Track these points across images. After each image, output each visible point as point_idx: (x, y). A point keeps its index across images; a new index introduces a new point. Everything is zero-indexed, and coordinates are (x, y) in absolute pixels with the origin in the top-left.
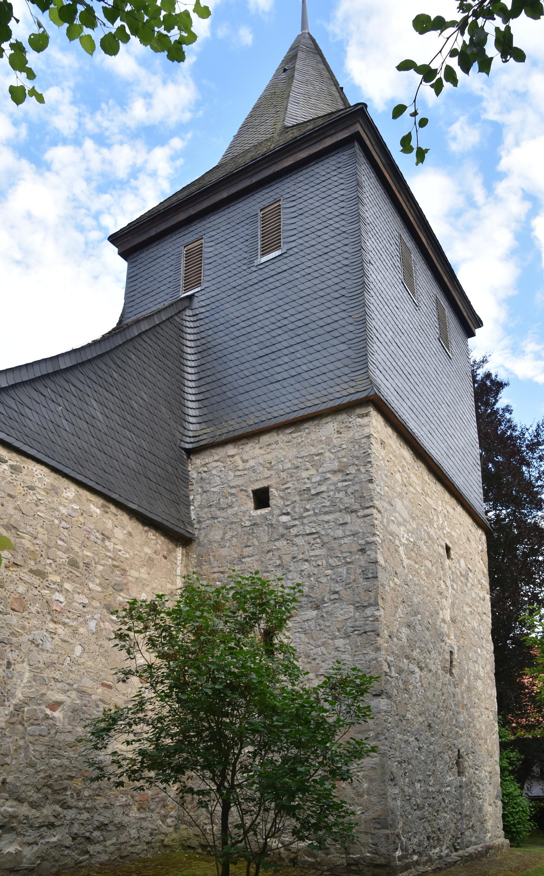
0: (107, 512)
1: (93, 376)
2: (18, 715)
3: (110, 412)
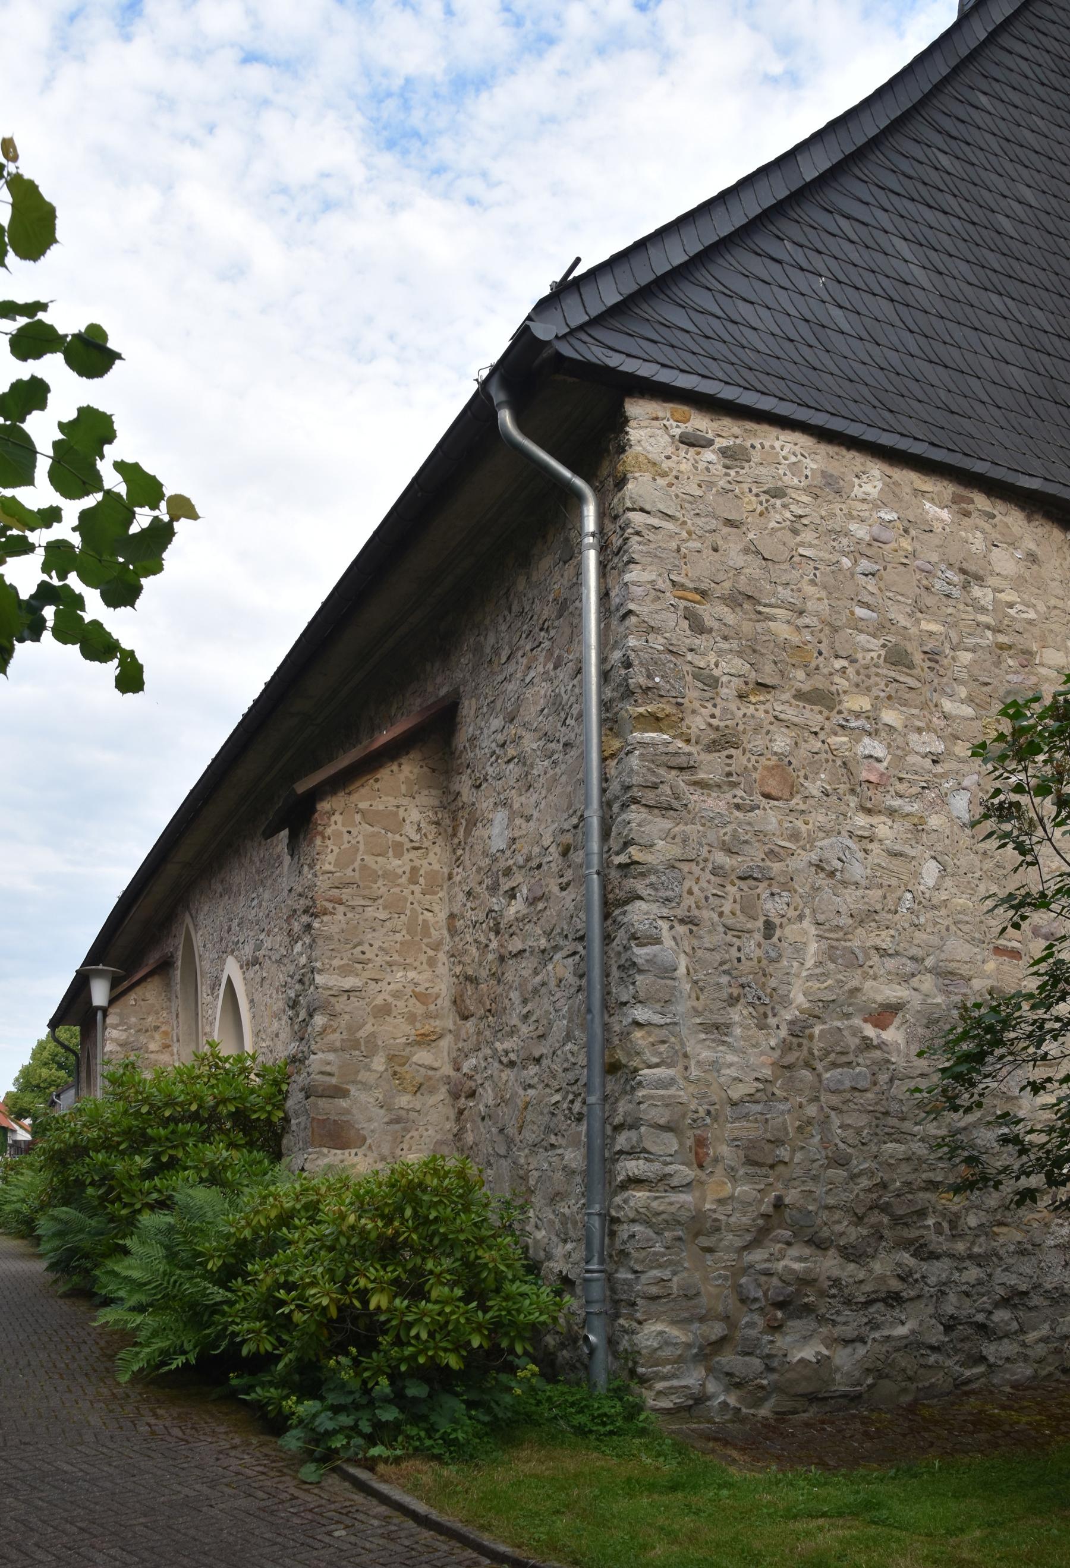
0: (967, 514)
1: (891, 181)
2: (800, 1045)
3: (945, 257)
